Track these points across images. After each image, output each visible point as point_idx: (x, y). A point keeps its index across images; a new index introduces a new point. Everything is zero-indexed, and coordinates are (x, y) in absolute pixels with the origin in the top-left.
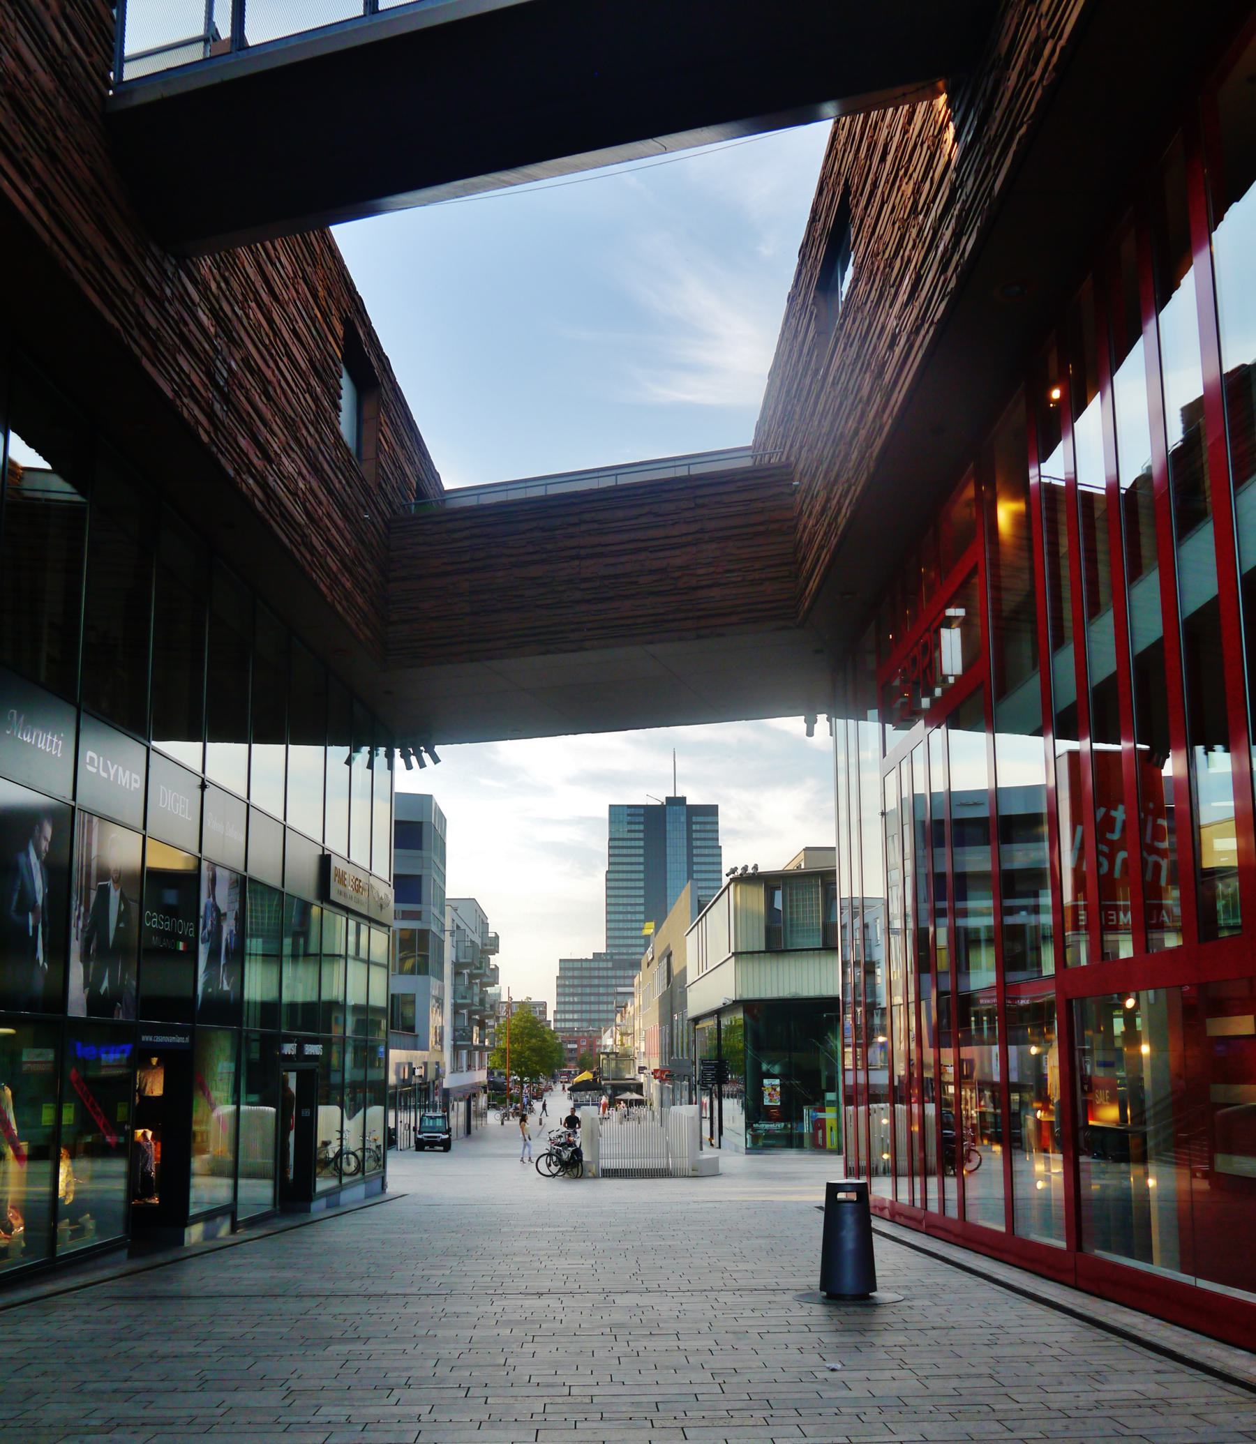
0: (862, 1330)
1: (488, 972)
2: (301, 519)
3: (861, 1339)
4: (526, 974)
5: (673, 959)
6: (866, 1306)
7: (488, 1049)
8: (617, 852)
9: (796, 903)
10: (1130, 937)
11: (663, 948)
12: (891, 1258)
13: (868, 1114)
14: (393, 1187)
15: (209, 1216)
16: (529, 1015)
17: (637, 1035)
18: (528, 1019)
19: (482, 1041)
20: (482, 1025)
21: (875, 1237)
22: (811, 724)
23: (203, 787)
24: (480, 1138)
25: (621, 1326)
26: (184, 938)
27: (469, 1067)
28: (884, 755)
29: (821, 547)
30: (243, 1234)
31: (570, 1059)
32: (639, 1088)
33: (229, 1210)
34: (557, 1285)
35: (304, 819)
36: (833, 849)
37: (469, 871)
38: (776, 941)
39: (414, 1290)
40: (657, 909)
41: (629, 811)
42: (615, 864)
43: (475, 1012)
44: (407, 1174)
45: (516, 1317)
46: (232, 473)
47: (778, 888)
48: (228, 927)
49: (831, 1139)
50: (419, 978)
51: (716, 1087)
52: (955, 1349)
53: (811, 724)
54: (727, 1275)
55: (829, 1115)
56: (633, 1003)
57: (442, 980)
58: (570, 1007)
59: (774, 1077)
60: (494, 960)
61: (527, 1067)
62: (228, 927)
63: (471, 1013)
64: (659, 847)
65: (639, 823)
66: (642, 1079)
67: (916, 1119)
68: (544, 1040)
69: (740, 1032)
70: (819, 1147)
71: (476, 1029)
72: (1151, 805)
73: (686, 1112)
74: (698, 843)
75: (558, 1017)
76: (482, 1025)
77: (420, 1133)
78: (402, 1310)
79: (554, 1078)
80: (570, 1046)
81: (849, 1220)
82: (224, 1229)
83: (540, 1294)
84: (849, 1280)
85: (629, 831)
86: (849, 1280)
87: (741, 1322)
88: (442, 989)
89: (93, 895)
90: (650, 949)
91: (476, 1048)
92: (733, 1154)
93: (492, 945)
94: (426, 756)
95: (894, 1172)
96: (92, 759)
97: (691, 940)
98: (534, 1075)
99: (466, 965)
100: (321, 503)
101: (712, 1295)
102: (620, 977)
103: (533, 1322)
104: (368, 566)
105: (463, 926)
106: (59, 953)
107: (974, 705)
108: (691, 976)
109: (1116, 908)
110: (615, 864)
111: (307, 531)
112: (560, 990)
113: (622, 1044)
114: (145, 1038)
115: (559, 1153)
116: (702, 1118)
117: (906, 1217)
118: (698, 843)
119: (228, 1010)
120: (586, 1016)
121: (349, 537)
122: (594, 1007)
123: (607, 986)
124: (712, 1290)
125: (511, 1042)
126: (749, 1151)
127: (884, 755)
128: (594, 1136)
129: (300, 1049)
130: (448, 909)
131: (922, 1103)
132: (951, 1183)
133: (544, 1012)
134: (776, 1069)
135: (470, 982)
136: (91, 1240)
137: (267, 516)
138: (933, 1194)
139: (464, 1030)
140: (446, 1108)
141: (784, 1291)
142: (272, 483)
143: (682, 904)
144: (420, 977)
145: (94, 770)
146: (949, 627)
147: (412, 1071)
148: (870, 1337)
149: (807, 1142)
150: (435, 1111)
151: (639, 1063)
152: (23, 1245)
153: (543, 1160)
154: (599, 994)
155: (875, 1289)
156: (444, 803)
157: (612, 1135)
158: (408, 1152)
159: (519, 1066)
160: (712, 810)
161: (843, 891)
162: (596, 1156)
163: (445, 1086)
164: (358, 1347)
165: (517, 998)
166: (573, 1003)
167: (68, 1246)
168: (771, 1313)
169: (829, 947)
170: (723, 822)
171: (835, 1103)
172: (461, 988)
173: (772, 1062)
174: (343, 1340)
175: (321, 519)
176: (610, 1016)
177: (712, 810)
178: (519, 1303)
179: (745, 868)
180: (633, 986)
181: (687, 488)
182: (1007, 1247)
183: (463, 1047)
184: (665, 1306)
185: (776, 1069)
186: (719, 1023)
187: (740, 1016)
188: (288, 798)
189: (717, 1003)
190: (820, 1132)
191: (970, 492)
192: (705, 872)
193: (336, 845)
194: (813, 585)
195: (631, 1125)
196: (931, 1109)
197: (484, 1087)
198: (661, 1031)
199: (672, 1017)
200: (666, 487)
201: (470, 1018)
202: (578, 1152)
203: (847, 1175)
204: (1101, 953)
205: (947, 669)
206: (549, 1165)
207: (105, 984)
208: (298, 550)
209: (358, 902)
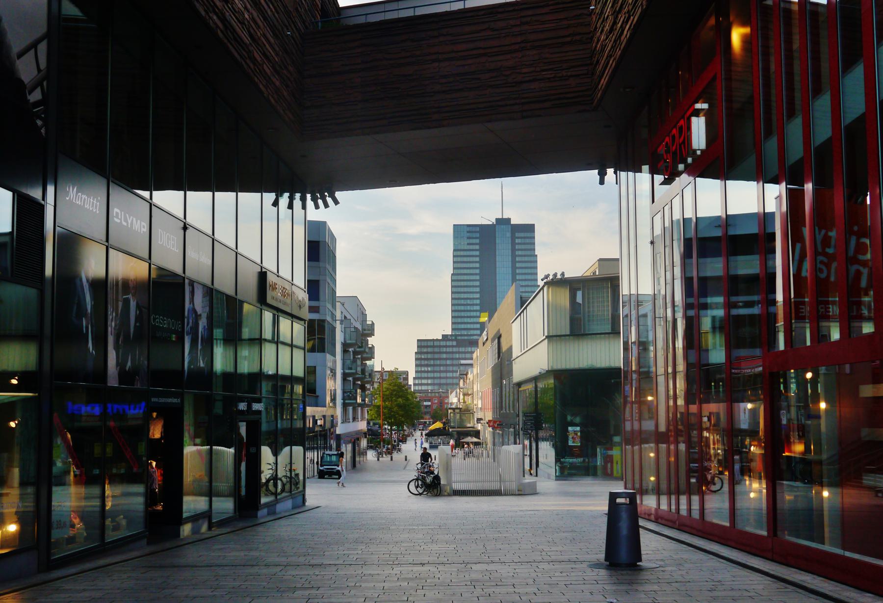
0: (631, 583)
1: (367, 350)
2: (247, 40)
3: (630, 587)
4: (393, 353)
5: (502, 340)
6: (635, 570)
7: (368, 406)
8: (459, 259)
9: (591, 299)
10: (838, 324)
11: (495, 332)
12: (653, 545)
13: (641, 449)
14: (310, 502)
15: (196, 518)
16: (396, 380)
17: (475, 393)
18: (396, 382)
19: (363, 400)
20: (363, 388)
21: (641, 531)
22: (602, 175)
23: (185, 228)
24: (362, 470)
25: (477, 581)
26: (175, 332)
27: (354, 419)
28: (653, 202)
29: (609, 56)
30: (216, 531)
31: (426, 413)
32: (477, 434)
33: (207, 515)
34: (432, 559)
35: (249, 249)
36: (618, 260)
37: (352, 279)
38: (577, 328)
39: (341, 562)
40: (490, 305)
41: (468, 229)
42: (458, 268)
43: (358, 379)
44: (318, 494)
45: (410, 576)
46: (203, 13)
47: (579, 289)
48: (203, 323)
49: (617, 469)
50: (318, 355)
51: (533, 433)
52: (688, 592)
53: (602, 175)
54: (544, 553)
55: (616, 453)
56: (472, 372)
57: (335, 356)
58: (425, 375)
59: (576, 425)
60: (371, 341)
61: (395, 418)
62: (203, 323)
63: (355, 380)
64: (490, 257)
65: (476, 238)
66: (479, 427)
67: (672, 453)
68: (407, 399)
69: (552, 393)
70: (608, 475)
71: (359, 391)
72: (856, 228)
73: (513, 450)
74: (520, 253)
75: (417, 382)
76: (363, 388)
77: (322, 466)
78: (336, 573)
79: (414, 426)
80: (425, 403)
81: (624, 516)
82: (204, 528)
83: (423, 564)
84: (623, 555)
85: (468, 244)
86: (623, 555)
87: (553, 579)
88: (335, 362)
89: (120, 304)
90: (485, 333)
91: (359, 405)
92: (547, 479)
93: (369, 331)
94: (329, 200)
95: (658, 492)
96: (117, 213)
97: (516, 327)
98: (400, 424)
99: (351, 345)
100: (259, 27)
101: (534, 564)
102: (462, 353)
103: (421, 579)
104: (290, 68)
105: (349, 317)
106: (101, 341)
107: (718, 164)
108: (516, 353)
109: (828, 303)
110: (458, 268)
111: (251, 48)
112: (418, 362)
113: (464, 402)
114: (154, 400)
115: (424, 478)
116: (524, 455)
117: (666, 520)
118: (520, 253)
119: (204, 378)
120: (437, 381)
121: (277, 49)
122: (443, 375)
123: (452, 359)
124: (535, 561)
125: (384, 401)
126: (558, 478)
127: (653, 202)
128: (448, 468)
129: (249, 406)
130: (338, 304)
132: (695, 499)
133: (406, 379)
134: (578, 420)
135: (354, 357)
136: (123, 533)
137: (226, 41)
138: (683, 507)
139: (350, 392)
140: (338, 447)
141: (581, 562)
142: (228, 18)
143: (508, 300)
144: (319, 354)
145: (118, 221)
146: (697, 116)
147: (315, 422)
148: (635, 587)
149: (599, 472)
150: (331, 450)
151: (476, 416)
152: (85, 534)
153: (412, 484)
154: (447, 365)
155: (640, 560)
156: (335, 227)
157: (457, 466)
158: (313, 480)
159: (390, 418)
160: (530, 228)
161: (624, 290)
162: (449, 483)
163: (337, 432)
164: (314, 592)
165: (387, 368)
166: (428, 372)
167: (111, 536)
168: (573, 574)
169: (615, 332)
170: (540, 236)
171: (620, 444)
172: (348, 362)
173: (574, 415)
174: (303, 588)
175: (259, 39)
176: (455, 381)
177: (530, 228)
178: (410, 569)
179: (555, 275)
180: (472, 359)
181: (514, 10)
182: (730, 536)
183: (350, 404)
184: (504, 571)
185: (578, 420)
186: (536, 387)
187: (552, 381)
188: (231, 230)
189: (535, 372)
190: (609, 465)
191: (712, 21)
193: (269, 265)
194: (604, 81)
195: (470, 461)
196: (682, 447)
197: (365, 434)
198: (493, 392)
199: (502, 383)
200: (500, 10)
201: (354, 383)
202: (437, 478)
204: (820, 337)
205: (695, 145)
206: (417, 487)
207: (129, 364)
208: (246, 62)
209: (285, 304)
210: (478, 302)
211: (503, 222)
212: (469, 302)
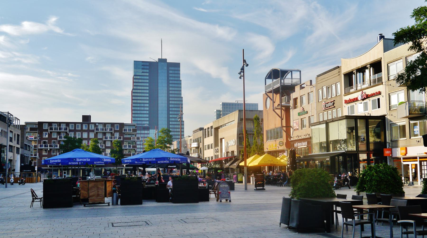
41: (143, 64)
85: (142, 72)
131: (334, 196)
177: (177, 65)
192: (175, 101)
203: (267, 132)
212: (142, 105)
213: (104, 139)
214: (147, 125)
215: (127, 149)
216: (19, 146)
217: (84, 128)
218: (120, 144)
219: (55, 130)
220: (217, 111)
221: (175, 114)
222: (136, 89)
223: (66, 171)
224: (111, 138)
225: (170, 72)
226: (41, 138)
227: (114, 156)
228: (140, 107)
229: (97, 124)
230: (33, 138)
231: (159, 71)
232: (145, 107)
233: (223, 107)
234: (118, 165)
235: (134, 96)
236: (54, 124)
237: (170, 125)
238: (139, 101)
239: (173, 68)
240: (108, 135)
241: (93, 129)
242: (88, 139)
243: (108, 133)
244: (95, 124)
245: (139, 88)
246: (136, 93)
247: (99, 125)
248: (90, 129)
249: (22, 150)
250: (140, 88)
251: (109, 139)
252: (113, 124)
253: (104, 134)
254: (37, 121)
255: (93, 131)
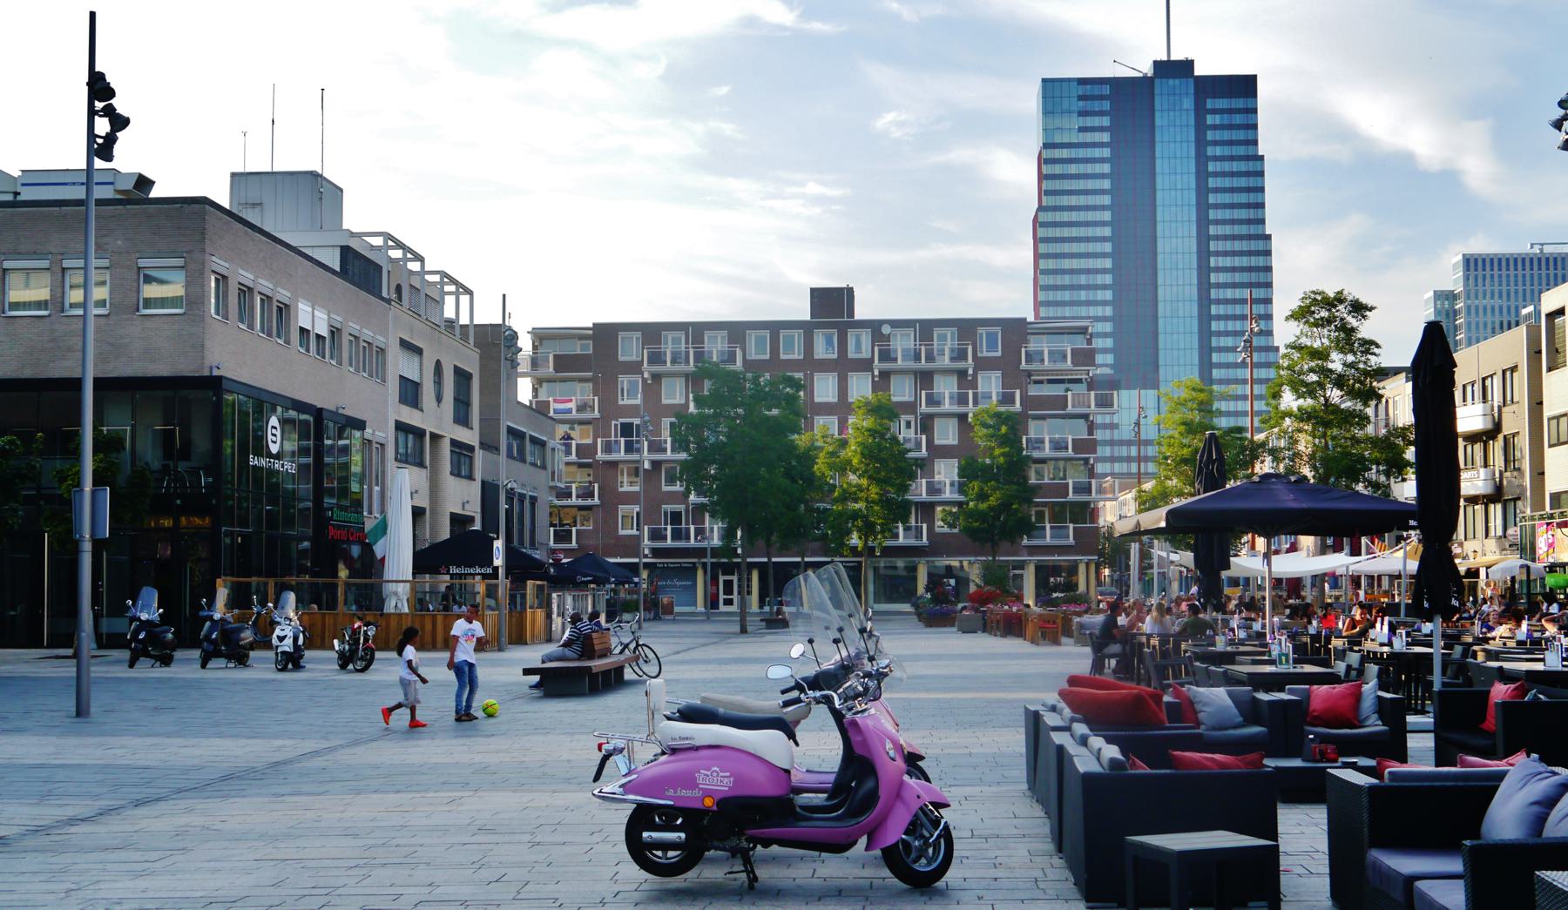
41: (1081, 90)
85: (1082, 129)
160: (1246, 86)
177: (1246, 86)
210: (1108, 279)
211: (1174, 70)
212: (1083, 279)
213: (924, 408)
214: (1108, 371)
215: (1043, 461)
216: (470, 436)
217: (821, 351)
218: (1010, 428)
219: (674, 362)
220: (1438, 295)
221: (1235, 318)
222: (1055, 209)
223: (735, 578)
224: (962, 400)
225: (1210, 119)
226: (610, 407)
227: (982, 497)
228: (1072, 287)
229: (886, 330)
230: (572, 405)
231: (1159, 121)
232: (1096, 287)
233: (1467, 278)
234: (1005, 545)
235: (1047, 240)
236: (670, 336)
237: (1211, 366)
238: (1067, 264)
239: (1222, 103)
240: (946, 387)
241: (866, 354)
242: (842, 408)
243: (946, 372)
244: (874, 326)
245: (1066, 200)
246: (1055, 224)
247: (899, 332)
248: (851, 355)
249: (490, 456)
250: (1073, 200)
251: (947, 406)
252: (966, 328)
253: (925, 378)
254: (586, 321)
255: (865, 365)
